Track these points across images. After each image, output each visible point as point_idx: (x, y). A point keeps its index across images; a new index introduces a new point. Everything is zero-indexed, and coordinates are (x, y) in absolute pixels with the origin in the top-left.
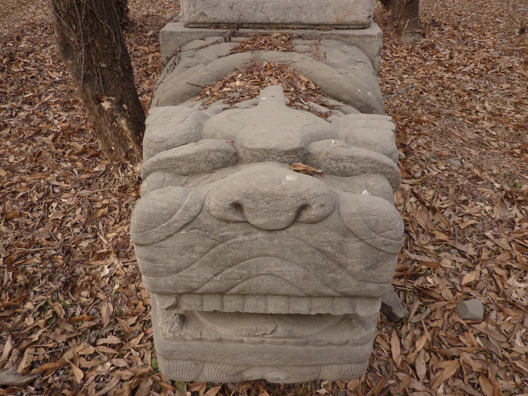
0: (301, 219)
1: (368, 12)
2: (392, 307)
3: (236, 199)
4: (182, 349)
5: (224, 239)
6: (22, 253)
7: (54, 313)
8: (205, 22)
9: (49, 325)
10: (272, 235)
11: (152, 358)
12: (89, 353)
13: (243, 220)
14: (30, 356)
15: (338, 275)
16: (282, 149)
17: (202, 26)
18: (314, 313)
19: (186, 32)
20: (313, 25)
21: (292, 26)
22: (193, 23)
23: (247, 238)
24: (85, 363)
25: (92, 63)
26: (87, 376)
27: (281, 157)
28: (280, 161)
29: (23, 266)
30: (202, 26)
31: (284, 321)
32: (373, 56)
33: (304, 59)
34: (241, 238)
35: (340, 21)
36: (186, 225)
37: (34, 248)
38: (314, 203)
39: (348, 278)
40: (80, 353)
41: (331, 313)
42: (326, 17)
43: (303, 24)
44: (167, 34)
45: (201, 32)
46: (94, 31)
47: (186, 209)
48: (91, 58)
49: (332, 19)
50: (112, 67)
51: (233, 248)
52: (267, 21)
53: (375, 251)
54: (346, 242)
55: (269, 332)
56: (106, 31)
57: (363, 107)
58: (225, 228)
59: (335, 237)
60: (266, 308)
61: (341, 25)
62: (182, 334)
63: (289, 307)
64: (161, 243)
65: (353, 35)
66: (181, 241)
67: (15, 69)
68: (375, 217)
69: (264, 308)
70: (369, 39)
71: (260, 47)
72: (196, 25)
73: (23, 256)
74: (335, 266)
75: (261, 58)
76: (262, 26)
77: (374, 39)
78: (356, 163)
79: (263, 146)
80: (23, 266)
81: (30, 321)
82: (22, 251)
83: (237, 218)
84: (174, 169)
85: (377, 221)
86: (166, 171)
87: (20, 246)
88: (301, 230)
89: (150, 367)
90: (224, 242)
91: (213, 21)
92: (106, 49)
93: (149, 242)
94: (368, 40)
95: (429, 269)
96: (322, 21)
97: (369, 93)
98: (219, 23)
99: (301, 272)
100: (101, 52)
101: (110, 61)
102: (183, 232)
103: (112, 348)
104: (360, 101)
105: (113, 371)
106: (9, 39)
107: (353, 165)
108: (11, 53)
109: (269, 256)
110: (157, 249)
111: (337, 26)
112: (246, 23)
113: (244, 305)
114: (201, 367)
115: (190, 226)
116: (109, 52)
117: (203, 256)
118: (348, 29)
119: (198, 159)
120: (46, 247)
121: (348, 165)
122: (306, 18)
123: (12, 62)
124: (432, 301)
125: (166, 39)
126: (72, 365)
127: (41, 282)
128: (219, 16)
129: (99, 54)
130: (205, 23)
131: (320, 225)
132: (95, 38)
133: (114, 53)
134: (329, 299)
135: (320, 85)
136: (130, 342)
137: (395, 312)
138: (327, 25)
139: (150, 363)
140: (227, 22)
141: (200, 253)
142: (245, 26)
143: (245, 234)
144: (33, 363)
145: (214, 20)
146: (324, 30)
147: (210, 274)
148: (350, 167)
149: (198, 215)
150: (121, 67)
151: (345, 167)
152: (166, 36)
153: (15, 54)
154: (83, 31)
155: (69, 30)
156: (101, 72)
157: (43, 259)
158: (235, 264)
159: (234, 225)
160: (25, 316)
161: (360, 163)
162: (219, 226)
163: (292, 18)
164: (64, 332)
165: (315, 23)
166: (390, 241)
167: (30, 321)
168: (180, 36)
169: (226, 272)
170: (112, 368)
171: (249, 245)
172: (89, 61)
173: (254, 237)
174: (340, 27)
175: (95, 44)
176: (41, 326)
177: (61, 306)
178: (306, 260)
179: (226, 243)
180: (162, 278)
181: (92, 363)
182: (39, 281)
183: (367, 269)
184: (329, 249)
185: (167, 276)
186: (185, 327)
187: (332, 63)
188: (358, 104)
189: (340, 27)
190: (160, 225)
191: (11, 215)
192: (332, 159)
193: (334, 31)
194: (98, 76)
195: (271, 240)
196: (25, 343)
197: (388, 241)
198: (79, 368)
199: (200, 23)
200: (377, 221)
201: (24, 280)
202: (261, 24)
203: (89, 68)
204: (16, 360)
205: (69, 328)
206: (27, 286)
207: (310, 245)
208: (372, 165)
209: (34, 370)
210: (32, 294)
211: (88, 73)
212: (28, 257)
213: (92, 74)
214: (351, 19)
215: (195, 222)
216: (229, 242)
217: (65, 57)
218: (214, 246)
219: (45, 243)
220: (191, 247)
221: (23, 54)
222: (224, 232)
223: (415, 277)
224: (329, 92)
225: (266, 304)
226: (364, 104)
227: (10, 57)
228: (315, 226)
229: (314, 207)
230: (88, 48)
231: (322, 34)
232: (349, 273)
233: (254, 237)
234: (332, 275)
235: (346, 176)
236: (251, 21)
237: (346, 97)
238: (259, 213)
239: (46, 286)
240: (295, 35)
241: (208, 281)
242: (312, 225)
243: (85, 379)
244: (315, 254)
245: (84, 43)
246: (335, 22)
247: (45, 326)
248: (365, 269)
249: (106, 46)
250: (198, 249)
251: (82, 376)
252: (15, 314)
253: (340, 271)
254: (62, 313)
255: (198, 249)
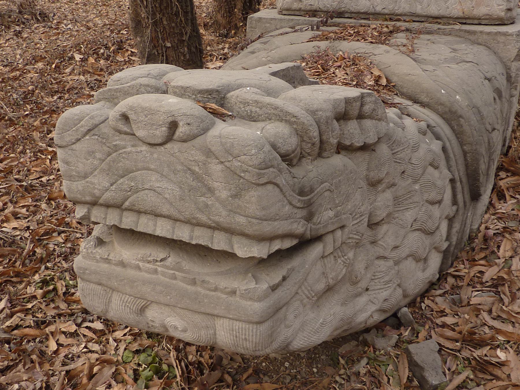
0: (176, 137)
1: (505, 4)
2: (426, 368)
3: (124, 110)
4: (93, 268)
5: (116, 148)
6: (50, 229)
7: (55, 289)
8: (301, 8)
9: (46, 298)
10: (153, 149)
11: (125, 349)
12: (70, 331)
13: (131, 132)
14: (18, 319)
15: (209, 200)
16: (197, 88)
17: (297, 13)
18: (194, 242)
19: (276, 19)
20: (431, 17)
21: (405, 18)
22: (287, 10)
23: (134, 149)
24: (63, 339)
25: (158, 42)
26: (60, 351)
27: (196, 95)
28: (194, 99)
29: (45, 242)
30: (297, 13)
31: (179, 255)
32: (509, 60)
33: (388, 52)
34: (129, 149)
35: (466, 13)
36: (89, 130)
37: (64, 227)
38: (182, 120)
39: (217, 205)
40: (63, 330)
41: (210, 246)
42: (448, 8)
43: (418, 16)
44: (255, 20)
45: (292, 20)
46: (162, 8)
47: (92, 118)
48: (158, 36)
49: (456, 10)
50: (177, 47)
51: (123, 158)
52: (373, 11)
53: (236, 177)
54: (209, 163)
55: (159, 259)
56: (175, 9)
57: (446, 113)
58: (117, 138)
59: (201, 158)
60: (155, 230)
61: (469, 18)
62: (94, 251)
63: (173, 232)
64: (73, 146)
65: (481, 32)
66: (86, 146)
67: (120, 58)
68: (231, 140)
69: (152, 228)
70: (503, 37)
71: (346, 37)
72: (290, 13)
73: (48, 233)
74: (204, 190)
75: (338, 49)
76: (367, 17)
77: (510, 38)
78: (261, 108)
79: (182, 85)
80: (45, 242)
81: (30, 290)
82: (50, 227)
83: (125, 129)
84: (113, 99)
85: (232, 145)
86: (108, 101)
87: (51, 223)
88: (175, 147)
89: (120, 358)
90: (117, 151)
91: (308, 8)
92: (173, 28)
93: (64, 144)
94: (502, 39)
95: (509, 342)
96: (446, 13)
97: (458, 97)
98: (316, 11)
99: (177, 192)
100: (168, 31)
101: (176, 42)
102: (87, 137)
103: (93, 332)
104: (441, 104)
105: (85, 353)
106: (125, 27)
107: (258, 109)
108: (121, 40)
109: (151, 170)
110: (70, 152)
111: (464, 20)
112: (347, 12)
113: (138, 223)
114: (109, 295)
115: (92, 133)
116: (176, 32)
117: (102, 164)
118: (480, 24)
119: (131, 91)
120: (74, 229)
121: (254, 109)
122: (422, 8)
123: (119, 51)
124: (489, 377)
125: (253, 26)
126: (51, 337)
127: (56, 259)
128: (317, 3)
129: (166, 32)
130: (300, 10)
131: (189, 144)
132: (163, 15)
133: (182, 33)
134: (209, 230)
135: (395, 82)
136: (114, 333)
137: (427, 375)
138: (450, 18)
139: (121, 355)
140: (325, 9)
141: (100, 159)
142: (346, 16)
143: (133, 146)
144: (17, 325)
145: (310, 7)
146: (445, 24)
147: (107, 182)
148: (256, 111)
149: (100, 124)
150: (188, 48)
151: (251, 112)
152: (254, 22)
153: (125, 43)
154: (152, 7)
155: (140, 6)
156: (166, 52)
157: (66, 241)
158: (126, 175)
159: (125, 136)
160: (29, 284)
161: (265, 109)
162: (114, 135)
163: (404, 8)
164: (57, 308)
165: (433, 15)
166: (247, 167)
167: (30, 290)
168: (269, 23)
169: (119, 182)
170: (85, 350)
171: (135, 157)
172: (154, 40)
173: (139, 149)
174: (468, 21)
175: (162, 22)
176: (38, 297)
177: (64, 284)
178: (180, 179)
179: (118, 152)
180: (75, 183)
181: (70, 341)
182: (55, 259)
183: (235, 196)
184: (197, 169)
185: (78, 181)
186: (99, 247)
187: (423, 59)
188: (440, 109)
189: (468, 21)
190: (72, 128)
191: (56, 195)
192: (241, 102)
193: (458, 27)
194: (163, 56)
195: (152, 154)
196: (18, 308)
197: (245, 167)
198: (56, 342)
199: (295, 10)
200: (232, 145)
201: (41, 253)
202: (365, 13)
203: (155, 46)
204: (4, 318)
205: (63, 306)
206: (41, 260)
207: (182, 163)
208: (276, 112)
209: (15, 332)
210: (43, 267)
211: (153, 52)
212: (54, 234)
213: (156, 53)
214: (482, 11)
215: (96, 129)
216: (121, 151)
217: (135, 33)
218: (109, 154)
219: (75, 225)
220: (93, 152)
221: (133, 43)
222: (116, 141)
223: (480, 344)
224: (405, 90)
225: (155, 225)
226: (447, 110)
227: (119, 46)
228: (185, 145)
229: (181, 124)
230: (156, 25)
231: (439, 29)
232: (218, 199)
233: (139, 149)
234: (203, 199)
235: (253, 121)
236: (353, 10)
237: (424, 98)
238: (139, 125)
239: (59, 265)
240: (403, 28)
241: (107, 190)
242: (183, 143)
243: (56, 352)
244: (186, 173)
245: (152, 19)
246: (461, 14)
247: (42, 299)
248: (231, 197)
249: (173, 25)
250: (98, 155)
251: (55, 349)
252: (21, 282)
253: (209, 195)
254: (61, 290)
255: (98, 155)
